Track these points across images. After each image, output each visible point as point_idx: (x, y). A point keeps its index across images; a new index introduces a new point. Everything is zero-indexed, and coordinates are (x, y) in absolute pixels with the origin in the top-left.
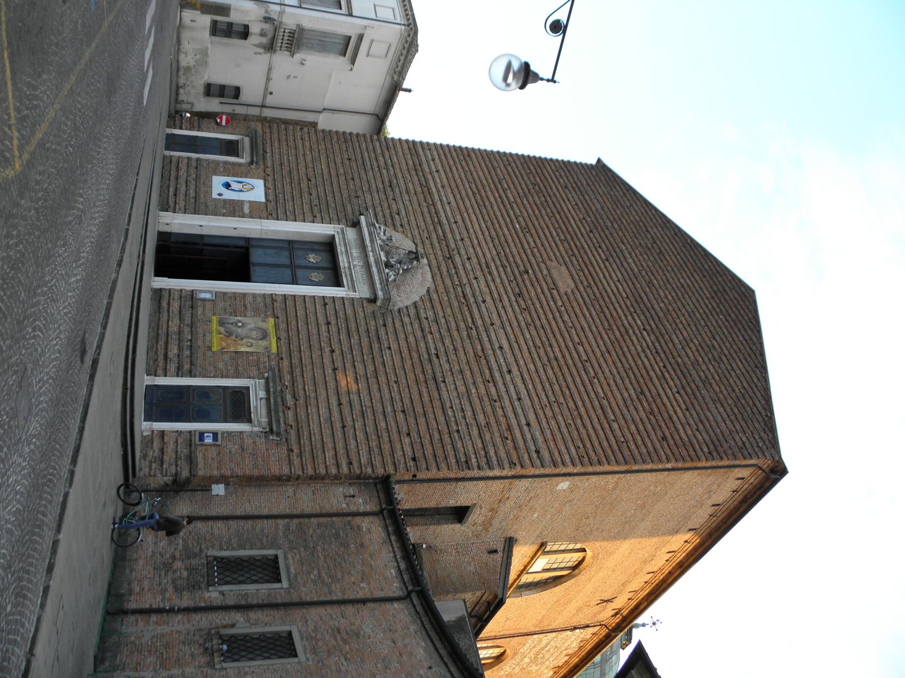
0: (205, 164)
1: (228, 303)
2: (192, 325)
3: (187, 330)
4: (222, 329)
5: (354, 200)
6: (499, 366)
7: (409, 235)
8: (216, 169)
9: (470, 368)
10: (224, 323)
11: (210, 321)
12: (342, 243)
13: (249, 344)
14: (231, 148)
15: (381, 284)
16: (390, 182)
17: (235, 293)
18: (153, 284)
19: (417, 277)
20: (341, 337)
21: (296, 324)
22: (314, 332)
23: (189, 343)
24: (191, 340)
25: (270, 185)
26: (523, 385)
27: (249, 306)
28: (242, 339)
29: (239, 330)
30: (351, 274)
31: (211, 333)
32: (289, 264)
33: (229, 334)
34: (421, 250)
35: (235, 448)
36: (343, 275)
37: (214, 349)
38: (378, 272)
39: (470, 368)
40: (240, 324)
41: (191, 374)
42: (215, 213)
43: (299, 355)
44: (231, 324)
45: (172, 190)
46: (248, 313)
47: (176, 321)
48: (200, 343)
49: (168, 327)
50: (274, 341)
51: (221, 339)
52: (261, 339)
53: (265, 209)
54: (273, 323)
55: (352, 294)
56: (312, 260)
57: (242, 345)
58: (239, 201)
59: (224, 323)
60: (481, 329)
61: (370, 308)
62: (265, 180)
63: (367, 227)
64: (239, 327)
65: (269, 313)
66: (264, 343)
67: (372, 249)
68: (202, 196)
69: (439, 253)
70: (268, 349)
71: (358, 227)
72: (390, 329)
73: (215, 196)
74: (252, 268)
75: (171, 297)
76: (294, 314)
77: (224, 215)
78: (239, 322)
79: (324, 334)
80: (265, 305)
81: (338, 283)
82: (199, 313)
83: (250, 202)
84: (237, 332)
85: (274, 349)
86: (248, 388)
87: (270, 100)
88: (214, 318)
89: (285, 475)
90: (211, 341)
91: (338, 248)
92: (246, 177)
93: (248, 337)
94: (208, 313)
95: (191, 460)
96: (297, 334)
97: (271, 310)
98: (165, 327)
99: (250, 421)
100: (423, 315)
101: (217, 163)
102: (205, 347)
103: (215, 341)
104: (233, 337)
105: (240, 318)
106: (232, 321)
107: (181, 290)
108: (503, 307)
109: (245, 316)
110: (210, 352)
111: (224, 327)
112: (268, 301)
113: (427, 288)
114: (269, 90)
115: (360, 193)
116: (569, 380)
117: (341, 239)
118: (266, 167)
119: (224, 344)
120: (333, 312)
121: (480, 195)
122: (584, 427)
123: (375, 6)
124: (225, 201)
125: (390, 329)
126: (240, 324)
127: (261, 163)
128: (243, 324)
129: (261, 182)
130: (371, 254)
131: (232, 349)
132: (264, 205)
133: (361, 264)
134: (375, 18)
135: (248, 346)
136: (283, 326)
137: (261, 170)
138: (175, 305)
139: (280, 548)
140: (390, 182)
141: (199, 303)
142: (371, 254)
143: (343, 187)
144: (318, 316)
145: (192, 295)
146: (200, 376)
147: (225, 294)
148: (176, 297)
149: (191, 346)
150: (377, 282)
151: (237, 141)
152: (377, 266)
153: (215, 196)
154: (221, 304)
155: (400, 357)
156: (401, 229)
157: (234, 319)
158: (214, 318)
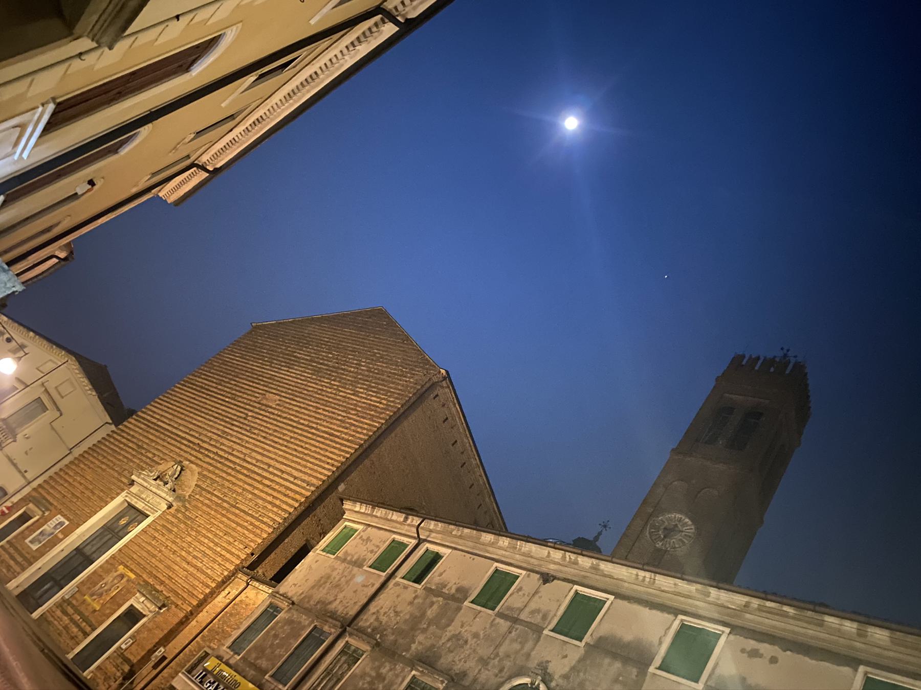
0: (14, 540)
4: (95, 597)
8: (23, 536)
11: (85, 600)
14: (24, 518)
16: (138, 445)
27: (102, 574)
29: (106, 588)
35: (145, 634)
40: (103, 586)
41: (94, 630)
42: (42, 555)
44: (99, 589)
46: (104, 577)
55: (157, 514)
60: (241, 463)
63: (139, 478)
77: (49, 551)
81: (147, 516)
86: (132, 605)
87: (29, 476)
88: (86, 597)
89: (183, 618)
95: (127, 660)
99: (144, 616)
101: (22, 532)
107: (54, 604)
109: (104, 579)
114: (23, 471)
116: (305, 439)
118: (56, 507)
119: (101, 602)
121: (364, 398)
123: (37, 369)
126: (103, 586)
127: (50, 507)
131: (108, 599)
134: (43, 375)
137: (54, 511)
138: (59, 613)
139: (204, 647)
140: (138, 445)
141: (71, 600)
146: (99, 626)
151: (25, 512)
154: (84, 588)
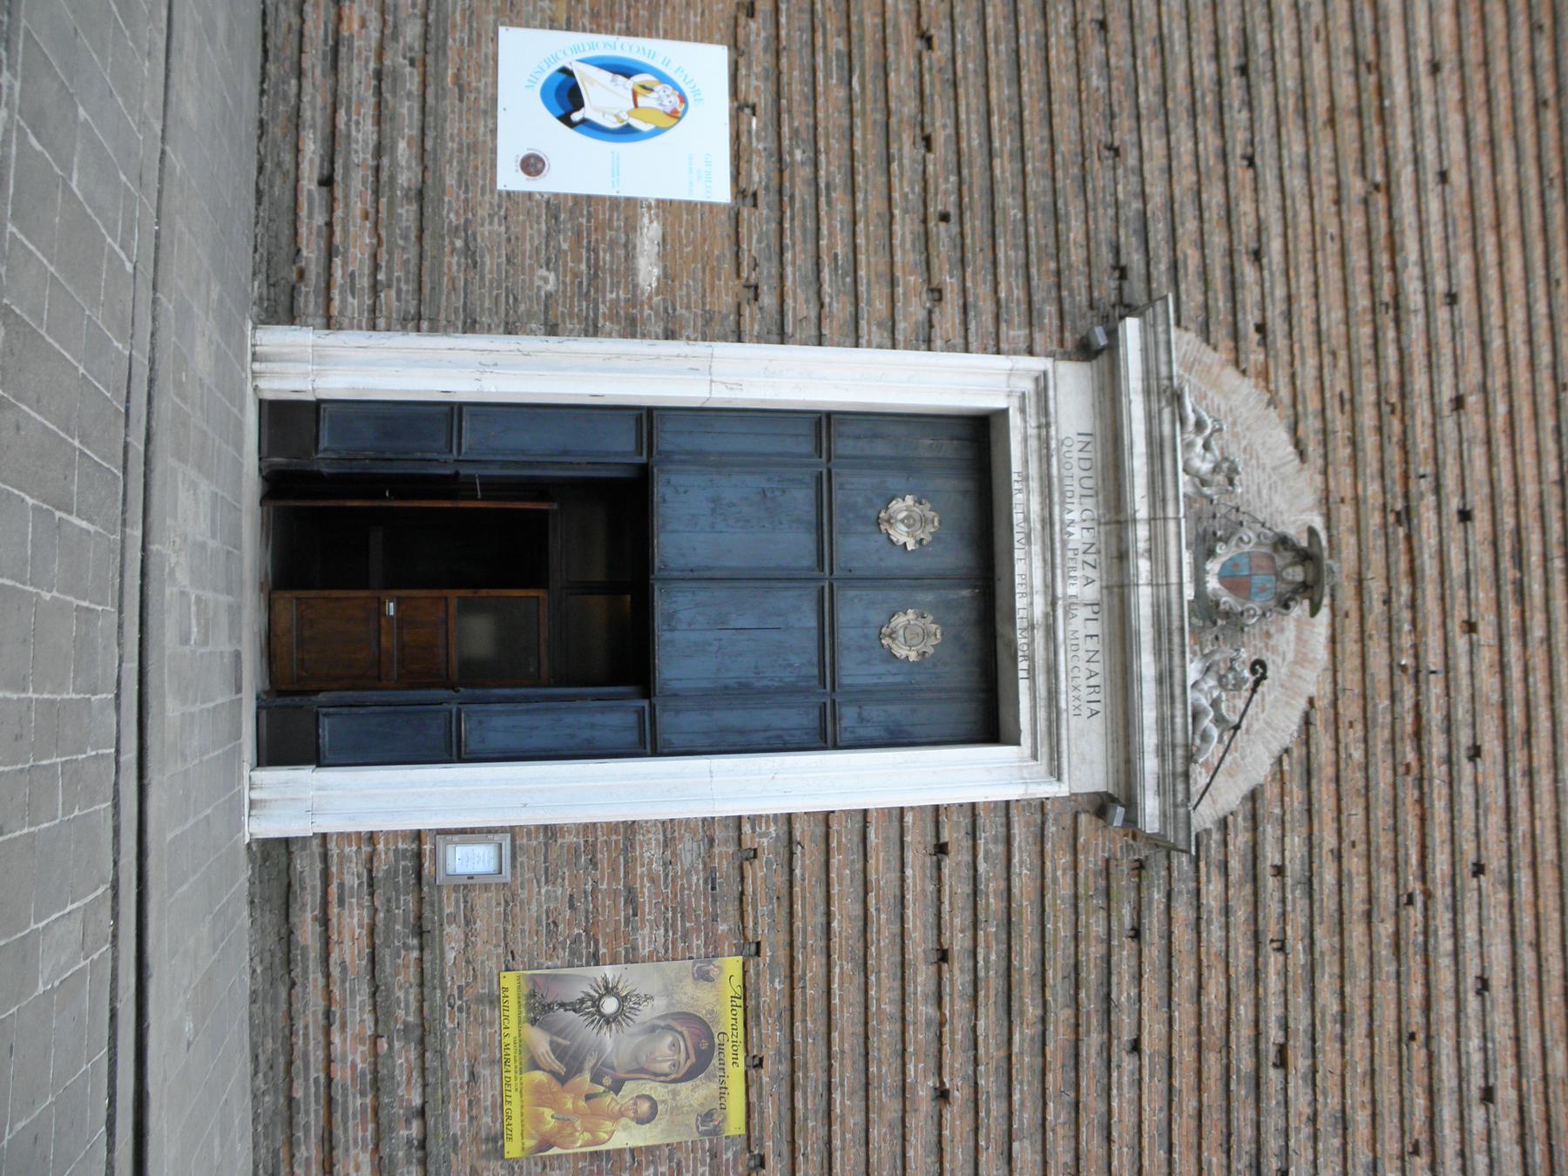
1: (561, 891)
2: (424, 1035)
3: (404, 1057)
4: (541, 1041)
5: (1099, 172)
6: (1461, 1076)
7: (1285, 393)
9: (1374, 1102)
10: (548, 1008)
11: (494, 1000)
12: (1034, 470)
13: (645, 1107)
15: (1161, 752)
17: (589, 828)
18: (263, 384)
19: (1283, 647)
20: (981, 1023)
21: (822, 972)
22: (886, 1007)
23: (415, 1129)
24: (422, 1113)
25: (757, 89)
26: (1517, 1150)
27: (645, 893)
28: (617, 1087)
30: (1052, 670)
31: (498, 1062)
32: (808, 560)
33: (569, 1063)
34: (1342, 566)
36: (1023, 665)
37: (513, 1149)
38: (1160, 680)
39: (1374, 1102)
43: (822, 1132)
44: (576, 1007)
45: (311, 147)
47: (359, 1017)
48: (457, 1122)
49: (329, 1060)
50: (735, 1075)
51: (541, 1096)
52: (690, 1075)
53: (728, 266)
54: (738, 973)
56: (900, 534)
57: (616, 1117)
58: (614, 203)
59: (548, 1008)
61: (1098, 842)
62: (738, 53)
64: (608, 1020)
65: (722, 928)
66: (695, 1094)
67: (1152, 538)
68: (450, 180)
69: (1373, 488)
70: (710, 1118)
71: (1103, 360)
72: (1153, 952)
73: (510, 178)
74: (662, 603)
75: (334, 889)
76: (820, 919)
78: (609, 990)
79: (922, 1010)
80: (711, 881)
82: (451, 956)
83: (668, 209)
84: (600, 1048)
85: (735, 1123)
88: (510, 981)
90: (499, 1106)
91: (1018, 498)
92: (650, 31)
93: (642, 1072)
94: (488, 955)
96: (823, 1029)
97: (732, 910)
98: (317, 1055)
100: (1271, 856)
102: (476, 1138)
103: (515, 1105)
104: (584, 1080)
105: (609, 972)
106: (576, 993)
108: (1530, 773)
109: (632, 957)
110: (495, 1165)
111: (547, 1027)
112: (724, 849)
113: (1302, 704)
115: (1124, 133)
117: (1033, 444)
120: (964, 889)
122: (1316, 296)
124: (554, 206)
125: (1153, 952)
126: (610, 1005)
128: (622, 1000)
129: (717, 57)
130: (1144, 565)
132: (724, 228)
133: (1091, 593)
135: (641, 1121)
136: (772, 990)
142: (1144, 565)
143: (1060, 55)
144: (909, 925)
145: (419, 855)
147: (550, 832)
148: (351, 881)
149: (423, 1145)
150: (1150, 739)
152: (1158, 653)
153: (510, 178)
155: (1163, 1086)
156: (1255, 357)
157: (585, 979)
158: (510, 981)
